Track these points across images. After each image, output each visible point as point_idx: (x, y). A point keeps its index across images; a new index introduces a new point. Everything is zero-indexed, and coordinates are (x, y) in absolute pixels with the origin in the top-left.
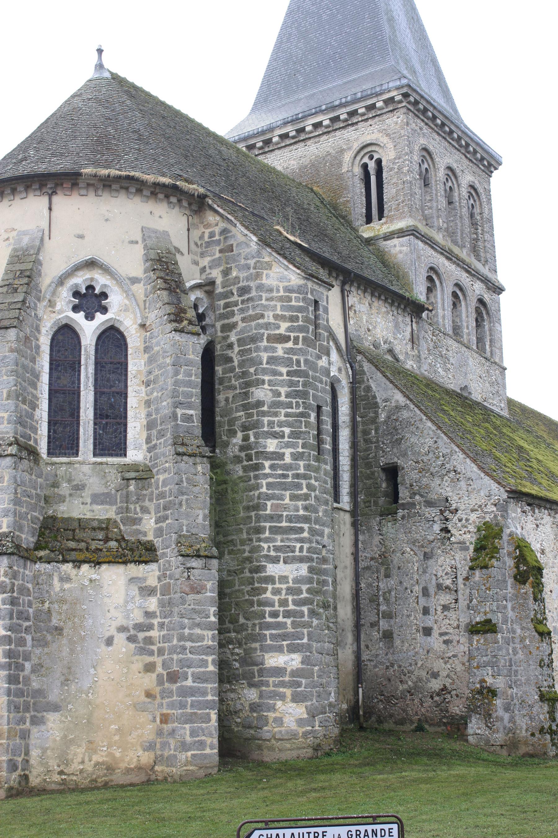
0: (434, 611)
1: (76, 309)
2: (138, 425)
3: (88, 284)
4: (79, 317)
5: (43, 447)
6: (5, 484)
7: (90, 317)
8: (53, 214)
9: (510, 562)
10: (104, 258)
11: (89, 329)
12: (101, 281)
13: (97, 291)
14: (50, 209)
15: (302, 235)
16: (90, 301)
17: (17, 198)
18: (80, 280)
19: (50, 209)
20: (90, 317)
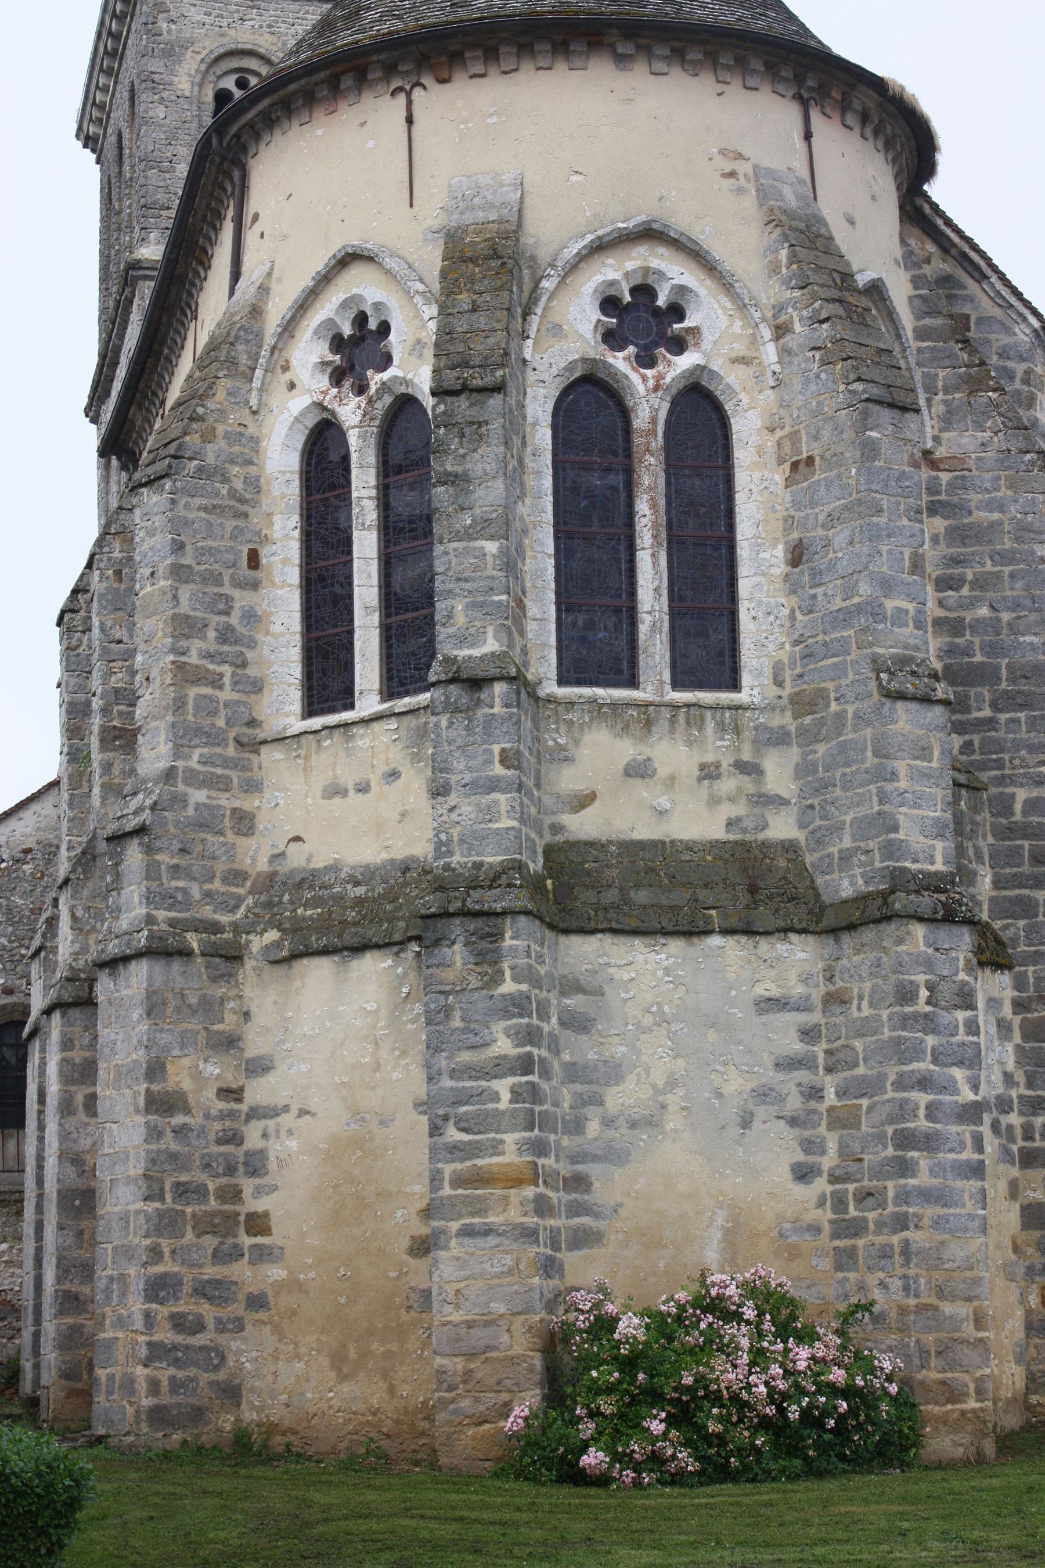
0: (477, 1332)
1: (612, 339)
2: (276, 628)
3: (638, 280)
4: (620, 361)
5: (544, 667)
6: (935, 764)
7: (646, 360)
8: (416, 129)
9: (428, 1231)
10: (682, 219)
11: (647, 394)
12: (675, 272)
13: (661, 302)
14: (410, 120)
15: (220, 217)
16: (644, 319)
17: (343, 105)
18: (616, 271)
19: (410, 120)
20: (646, 360)
